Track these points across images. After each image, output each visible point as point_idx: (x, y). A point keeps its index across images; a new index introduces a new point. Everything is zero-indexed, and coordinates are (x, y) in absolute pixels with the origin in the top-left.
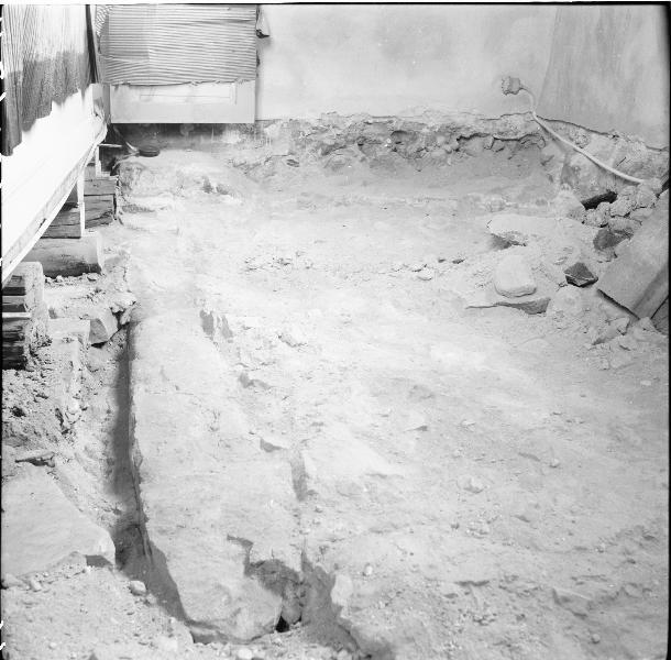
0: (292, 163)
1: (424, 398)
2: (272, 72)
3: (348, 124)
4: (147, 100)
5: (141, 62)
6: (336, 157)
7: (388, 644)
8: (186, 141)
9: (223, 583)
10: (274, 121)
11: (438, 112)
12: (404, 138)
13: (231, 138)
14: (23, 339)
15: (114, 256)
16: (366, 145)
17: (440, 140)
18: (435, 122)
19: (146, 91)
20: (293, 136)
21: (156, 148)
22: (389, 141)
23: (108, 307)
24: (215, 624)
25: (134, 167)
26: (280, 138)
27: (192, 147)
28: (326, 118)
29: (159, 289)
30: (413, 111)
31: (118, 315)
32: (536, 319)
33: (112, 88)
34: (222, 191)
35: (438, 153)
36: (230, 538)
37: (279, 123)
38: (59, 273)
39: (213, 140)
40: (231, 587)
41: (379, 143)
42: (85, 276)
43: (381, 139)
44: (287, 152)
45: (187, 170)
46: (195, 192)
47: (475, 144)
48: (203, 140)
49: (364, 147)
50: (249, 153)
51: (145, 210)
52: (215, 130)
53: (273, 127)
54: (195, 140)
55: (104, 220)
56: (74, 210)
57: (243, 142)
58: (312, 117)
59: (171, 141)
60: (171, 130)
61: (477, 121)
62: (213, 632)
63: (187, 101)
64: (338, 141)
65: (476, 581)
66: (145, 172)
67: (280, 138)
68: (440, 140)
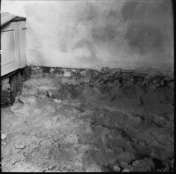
3: (114, 73)
11: (154, 69)
17: (155, 81)
18: (152, 74)
20: (91, 76)
26: (86, 76)
29: (130, 72)
30: (142, 68)
44: (88, 81)
57: (72, 76)
64: (109, 79)
67: (86, 76)
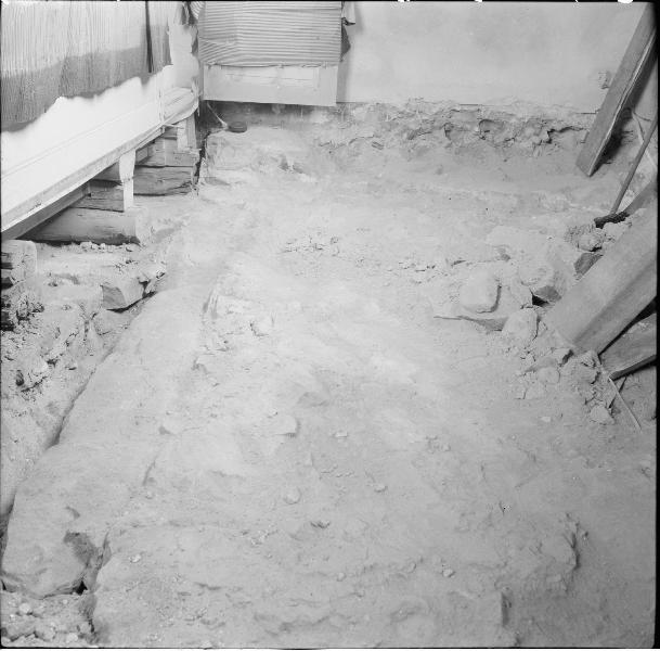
0: (375, 145)
1: (315, 405)
2: (360, 55)
4: (237, 81)
5: (228, 44)
6: (421, 142)
7: (107, 624)
8: (276, 119)
9: (41, 545)
10: (361, 104)
12: (493, 128)
13: (319, 118)
14: (9, 306)
15: (172, 226)
16: (453, 132)
17: (529, 131)
18: (524, 113)
19: (237, 72)
20: (379, 119)
21: (243, 124)
22: (477, 129)
23: (134, 276)
24: (22, 578)
25: (218, 142)
27: (282, 125)
28: (413, 104)
31: (145, 284)
32: (495, 335)
33: (206, 68)
34: (297, 170)
35: (526, 145)
36: (68, 508)
37: (367, 106)
38: (103, 241)
39: (301, 119)
40: (46, 550)
41: (466, 130)
42: (125, 246)
43: (468, 126)
45: (266, 147)
46: (272, 169)
47: (567, 137)
48: (293, 119)
49: (451, 134)
50: (335, 134)
51: (223, 183)
52: (304, 110)
53: (360, 110)
54: (285, 118)
55: (183, 190)
56: (119, 187)
58: (399, 103)
59: (263, 117)
60: (264, 108)
61: (570, 115)
62: (18, 584)
63: (273, 83)
64: (423, 127)
65: (210, 585)
66: (228, 148)
68: (529, 131)
